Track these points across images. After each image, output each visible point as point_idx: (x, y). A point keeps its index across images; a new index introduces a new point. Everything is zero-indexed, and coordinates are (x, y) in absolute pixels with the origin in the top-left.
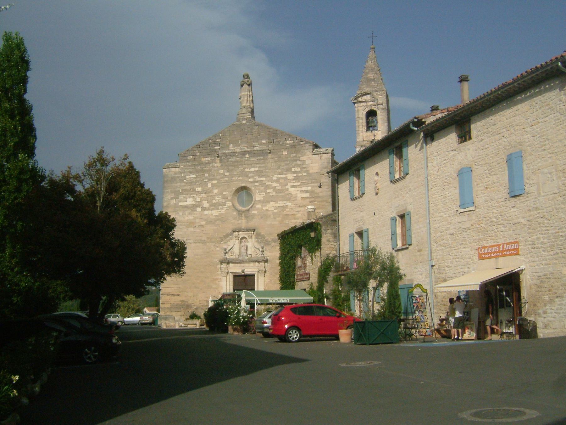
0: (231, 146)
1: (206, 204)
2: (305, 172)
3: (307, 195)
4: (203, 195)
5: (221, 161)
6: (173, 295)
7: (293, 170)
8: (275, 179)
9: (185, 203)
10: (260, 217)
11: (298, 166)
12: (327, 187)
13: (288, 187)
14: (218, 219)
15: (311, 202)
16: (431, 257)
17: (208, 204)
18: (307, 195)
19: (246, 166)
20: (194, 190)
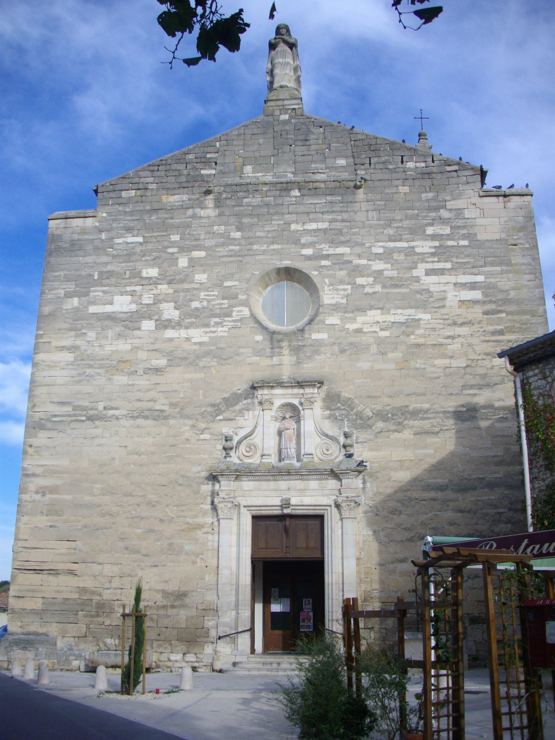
0: (248, 169)
1: (169, 311)
2: (464, 237)
3: (477, 295)
4: (163, 288)
5: (218, 203)
6: (54, 572)
7: (430, 231)
8: (381, 251)
9: (108, 309)
10: (336, 348)
11: (443, 221)
13: (419, 271)
14: (207, 354)
15: (486, 313)
17: (177, 313)
18: (477, 295)
19: (293, 217)
20: (136, 274)
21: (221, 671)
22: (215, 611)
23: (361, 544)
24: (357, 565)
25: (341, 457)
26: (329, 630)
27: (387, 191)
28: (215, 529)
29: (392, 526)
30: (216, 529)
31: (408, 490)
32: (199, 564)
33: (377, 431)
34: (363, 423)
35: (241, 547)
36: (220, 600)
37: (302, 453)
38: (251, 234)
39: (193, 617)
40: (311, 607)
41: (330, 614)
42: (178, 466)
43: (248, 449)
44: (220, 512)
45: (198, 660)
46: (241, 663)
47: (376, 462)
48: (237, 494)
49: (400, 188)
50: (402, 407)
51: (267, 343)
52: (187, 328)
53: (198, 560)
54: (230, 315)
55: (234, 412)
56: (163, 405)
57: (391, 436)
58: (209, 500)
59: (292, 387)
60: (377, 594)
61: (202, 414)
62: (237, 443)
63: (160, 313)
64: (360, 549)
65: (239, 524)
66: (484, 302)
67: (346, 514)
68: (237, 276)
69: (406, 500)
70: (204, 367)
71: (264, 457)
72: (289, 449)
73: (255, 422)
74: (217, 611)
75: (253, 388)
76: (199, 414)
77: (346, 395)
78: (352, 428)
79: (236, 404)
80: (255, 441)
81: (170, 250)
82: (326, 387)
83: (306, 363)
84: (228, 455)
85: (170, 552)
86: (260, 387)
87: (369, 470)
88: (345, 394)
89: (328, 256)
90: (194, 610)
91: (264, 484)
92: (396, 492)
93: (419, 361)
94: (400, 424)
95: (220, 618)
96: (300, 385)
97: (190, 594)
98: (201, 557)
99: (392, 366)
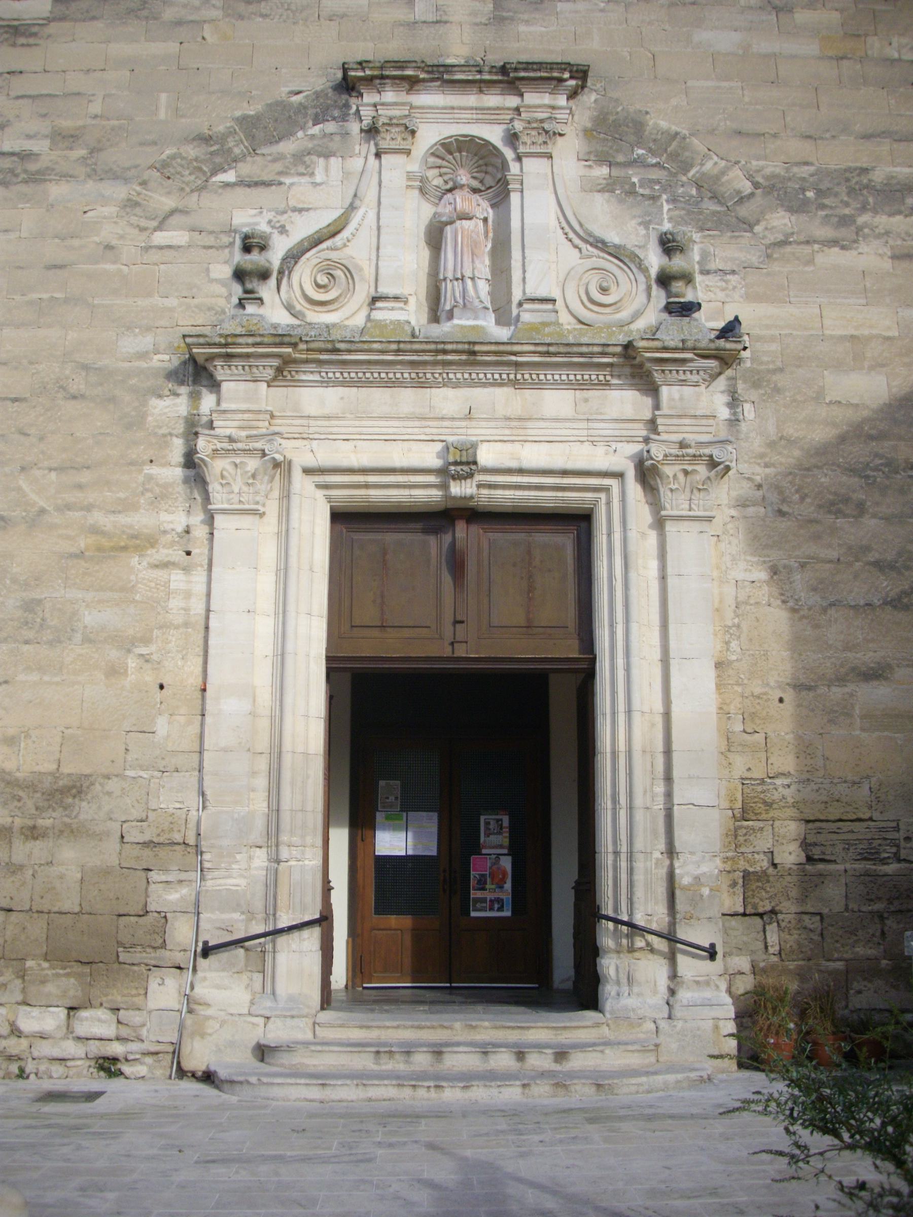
16: (179, 844)
21: (208, 1077)
22: (188, 849)
23: (729, 614)
24: (719, 686)
25: (652, 316)
26: (617, 921)
28: (196, 552)
29: (834, 554)
30: (201, 552)
31: (881, 436)
32: (132, 678)
33: (771, 238)
35: (291, 614)
36: (211, 809)
37: (517, 295)
39: (106, 872)
40: (506, 842)
41: (624, 865)
42: (72, 335)
43: (323, 279)
44: (214, 487)
45: (124, 1032)
46: (289, 1048)
47: (772, 339)
48: (280, 425)
50: (848, 170)
53: (132, 663)
55: (275, 160)
56: (29, 137)
57: (820, 259)
58: (178, 447)
59: (481, 86)
60: (787, 792)
61: (165, 165)
62: (284, 259)
64: (727, 629)
65: (284, 536)
67: (675, 502)
69: (876, 469)
70: (179, 23)
71: (379, 304)
72: (469, 283)
73: (351, 193)
74: (199, 852)
75: (348, 86)
76: (152, 167)
77: (663, 124)
78: (687, 224)
79: (288, 134)
80: (348, 251)
82: (593, 97)
83: (527, 22)
84: (249, 297)
85: (30, 634)
86: (370, 80)
87: (748, 364)
88: (660, 121)
90: (113, 844)
91: (379, 398)
92: (842, 439)
93: (895, 40)
94: (845, 221)
95: (209, 875)
96: (510, 77)
97: (98, 787)
98: (144, 650)
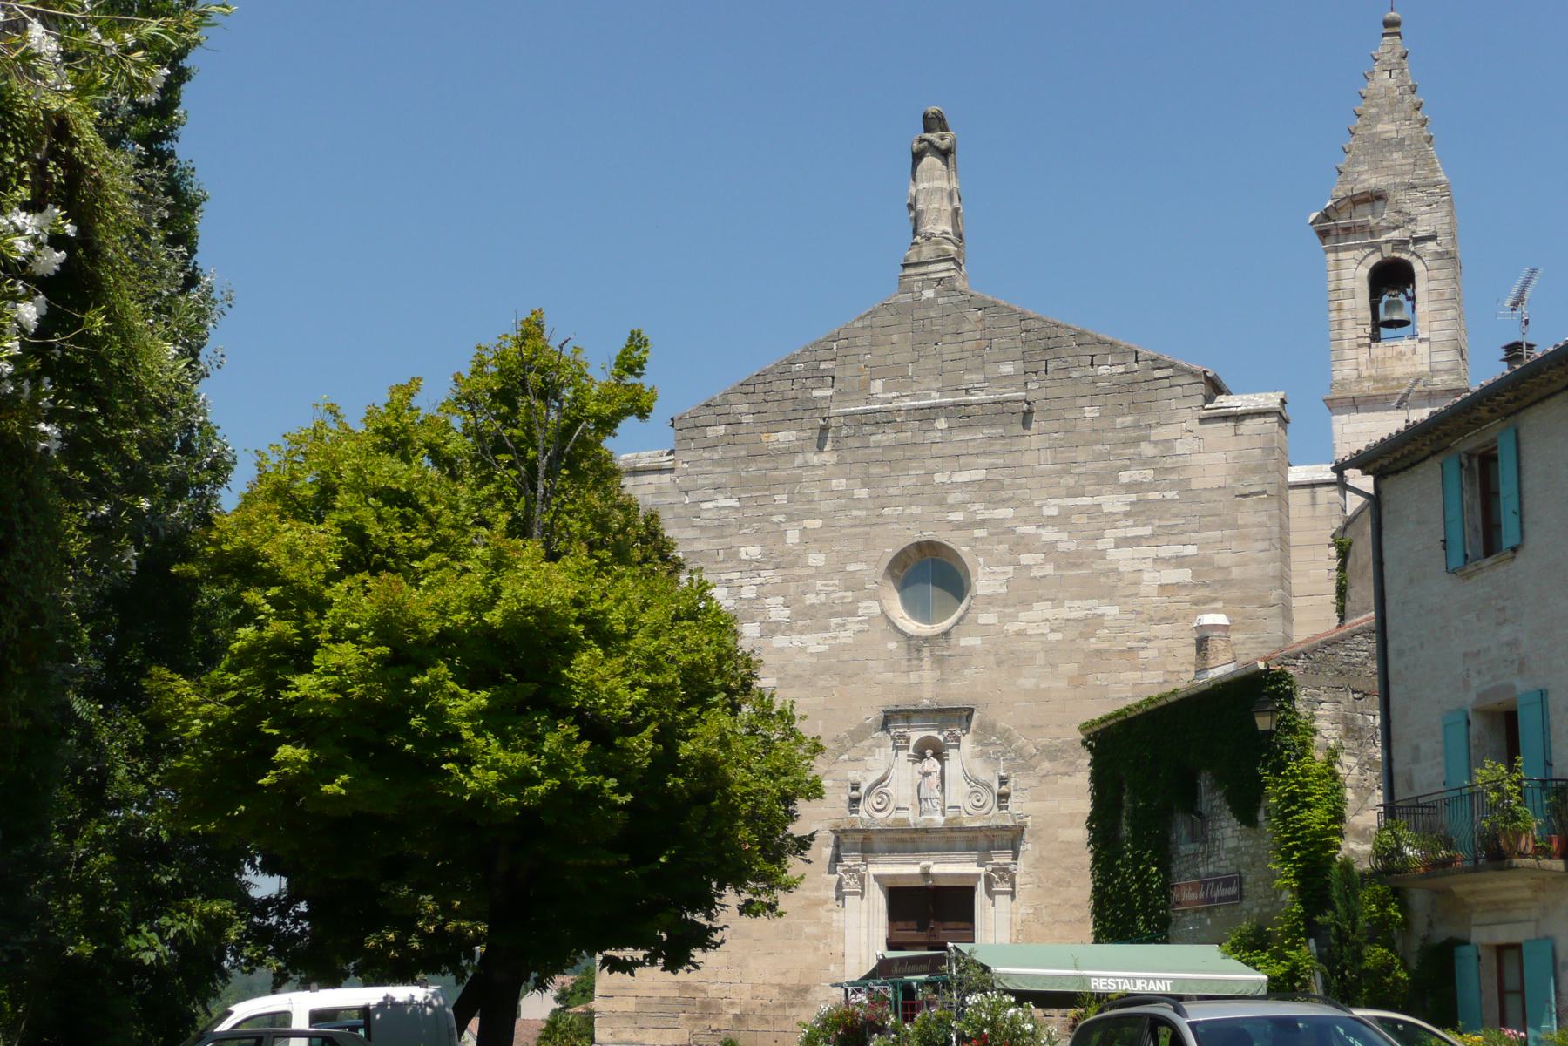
3: (1184, 575)
7: (1125, 477)
8: (1054, 512)
11: (1145, 462)
12: (1266, 544)
17: (787, 612)
18: (1184, 575)
27: (1069, 415)
34: (1023, 762)
38: (881, 492)
49: (1087, 409)
51: (903, 653)
52: (801, 633)
54: (854, 614)
63: (766, 610)
66: (1195, 585)
68: (863, 556)
81: (775, 519)
89: (984, 521)
94: (1072, 763)
99: (1063, 684)
